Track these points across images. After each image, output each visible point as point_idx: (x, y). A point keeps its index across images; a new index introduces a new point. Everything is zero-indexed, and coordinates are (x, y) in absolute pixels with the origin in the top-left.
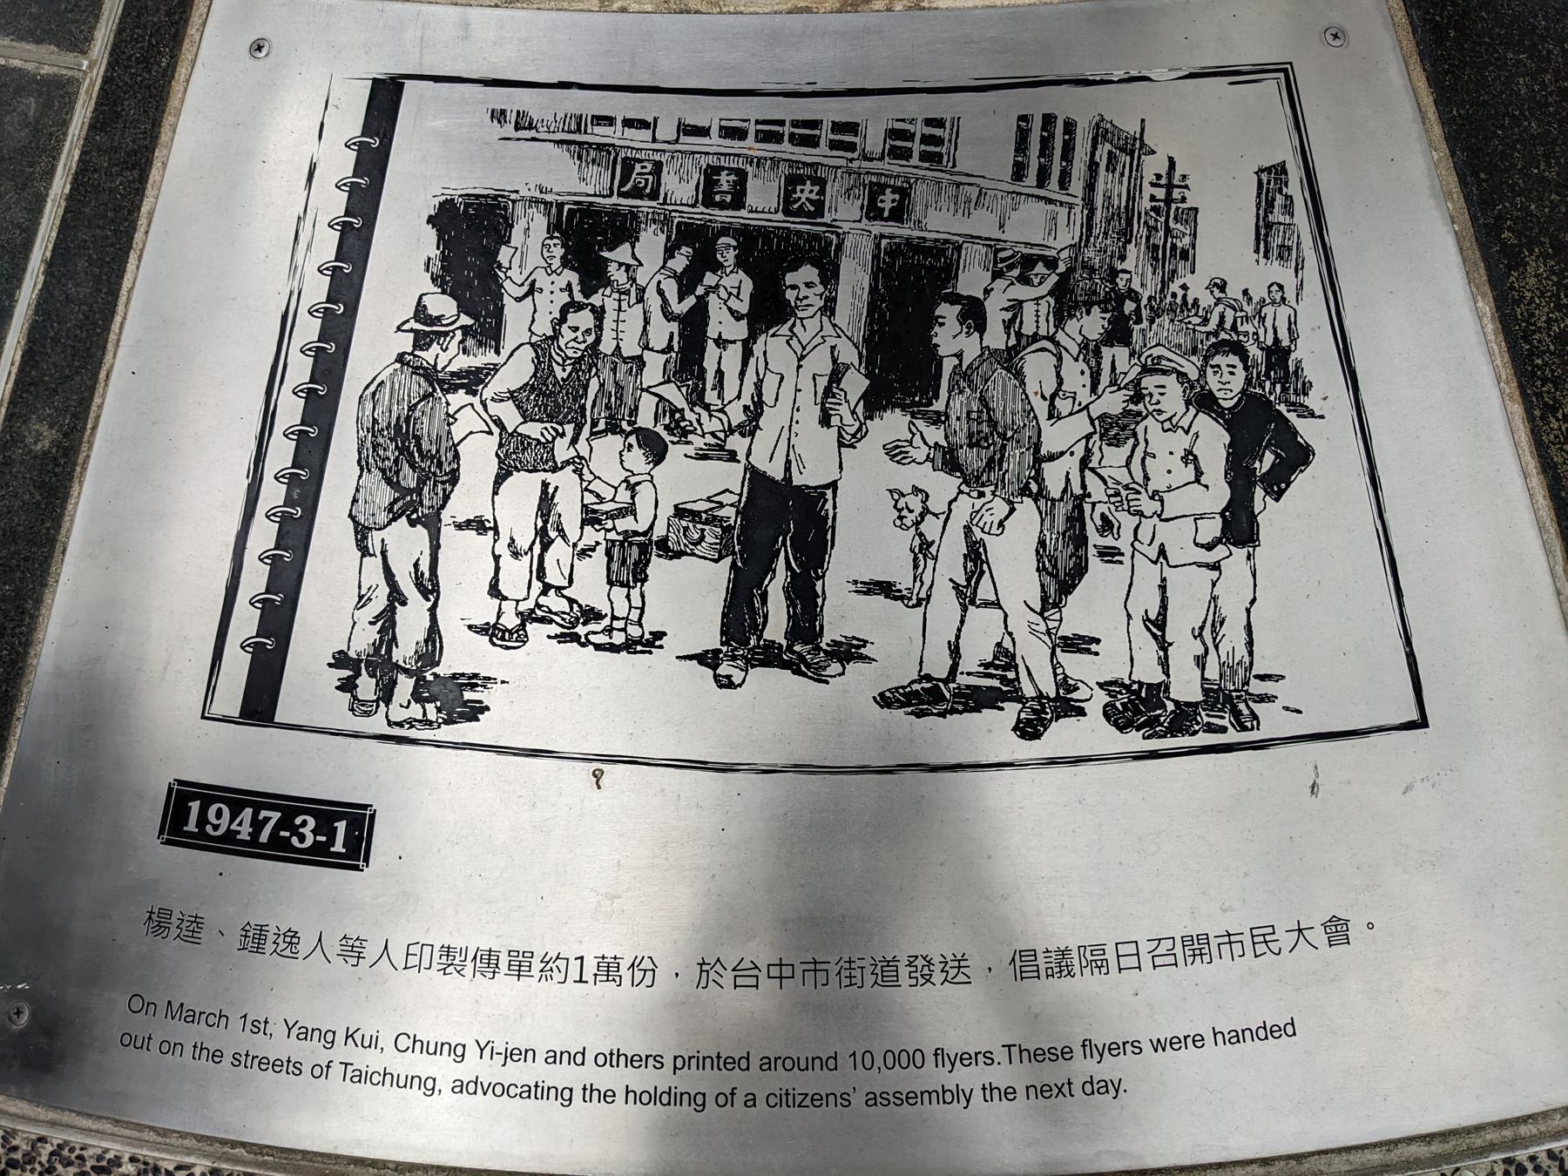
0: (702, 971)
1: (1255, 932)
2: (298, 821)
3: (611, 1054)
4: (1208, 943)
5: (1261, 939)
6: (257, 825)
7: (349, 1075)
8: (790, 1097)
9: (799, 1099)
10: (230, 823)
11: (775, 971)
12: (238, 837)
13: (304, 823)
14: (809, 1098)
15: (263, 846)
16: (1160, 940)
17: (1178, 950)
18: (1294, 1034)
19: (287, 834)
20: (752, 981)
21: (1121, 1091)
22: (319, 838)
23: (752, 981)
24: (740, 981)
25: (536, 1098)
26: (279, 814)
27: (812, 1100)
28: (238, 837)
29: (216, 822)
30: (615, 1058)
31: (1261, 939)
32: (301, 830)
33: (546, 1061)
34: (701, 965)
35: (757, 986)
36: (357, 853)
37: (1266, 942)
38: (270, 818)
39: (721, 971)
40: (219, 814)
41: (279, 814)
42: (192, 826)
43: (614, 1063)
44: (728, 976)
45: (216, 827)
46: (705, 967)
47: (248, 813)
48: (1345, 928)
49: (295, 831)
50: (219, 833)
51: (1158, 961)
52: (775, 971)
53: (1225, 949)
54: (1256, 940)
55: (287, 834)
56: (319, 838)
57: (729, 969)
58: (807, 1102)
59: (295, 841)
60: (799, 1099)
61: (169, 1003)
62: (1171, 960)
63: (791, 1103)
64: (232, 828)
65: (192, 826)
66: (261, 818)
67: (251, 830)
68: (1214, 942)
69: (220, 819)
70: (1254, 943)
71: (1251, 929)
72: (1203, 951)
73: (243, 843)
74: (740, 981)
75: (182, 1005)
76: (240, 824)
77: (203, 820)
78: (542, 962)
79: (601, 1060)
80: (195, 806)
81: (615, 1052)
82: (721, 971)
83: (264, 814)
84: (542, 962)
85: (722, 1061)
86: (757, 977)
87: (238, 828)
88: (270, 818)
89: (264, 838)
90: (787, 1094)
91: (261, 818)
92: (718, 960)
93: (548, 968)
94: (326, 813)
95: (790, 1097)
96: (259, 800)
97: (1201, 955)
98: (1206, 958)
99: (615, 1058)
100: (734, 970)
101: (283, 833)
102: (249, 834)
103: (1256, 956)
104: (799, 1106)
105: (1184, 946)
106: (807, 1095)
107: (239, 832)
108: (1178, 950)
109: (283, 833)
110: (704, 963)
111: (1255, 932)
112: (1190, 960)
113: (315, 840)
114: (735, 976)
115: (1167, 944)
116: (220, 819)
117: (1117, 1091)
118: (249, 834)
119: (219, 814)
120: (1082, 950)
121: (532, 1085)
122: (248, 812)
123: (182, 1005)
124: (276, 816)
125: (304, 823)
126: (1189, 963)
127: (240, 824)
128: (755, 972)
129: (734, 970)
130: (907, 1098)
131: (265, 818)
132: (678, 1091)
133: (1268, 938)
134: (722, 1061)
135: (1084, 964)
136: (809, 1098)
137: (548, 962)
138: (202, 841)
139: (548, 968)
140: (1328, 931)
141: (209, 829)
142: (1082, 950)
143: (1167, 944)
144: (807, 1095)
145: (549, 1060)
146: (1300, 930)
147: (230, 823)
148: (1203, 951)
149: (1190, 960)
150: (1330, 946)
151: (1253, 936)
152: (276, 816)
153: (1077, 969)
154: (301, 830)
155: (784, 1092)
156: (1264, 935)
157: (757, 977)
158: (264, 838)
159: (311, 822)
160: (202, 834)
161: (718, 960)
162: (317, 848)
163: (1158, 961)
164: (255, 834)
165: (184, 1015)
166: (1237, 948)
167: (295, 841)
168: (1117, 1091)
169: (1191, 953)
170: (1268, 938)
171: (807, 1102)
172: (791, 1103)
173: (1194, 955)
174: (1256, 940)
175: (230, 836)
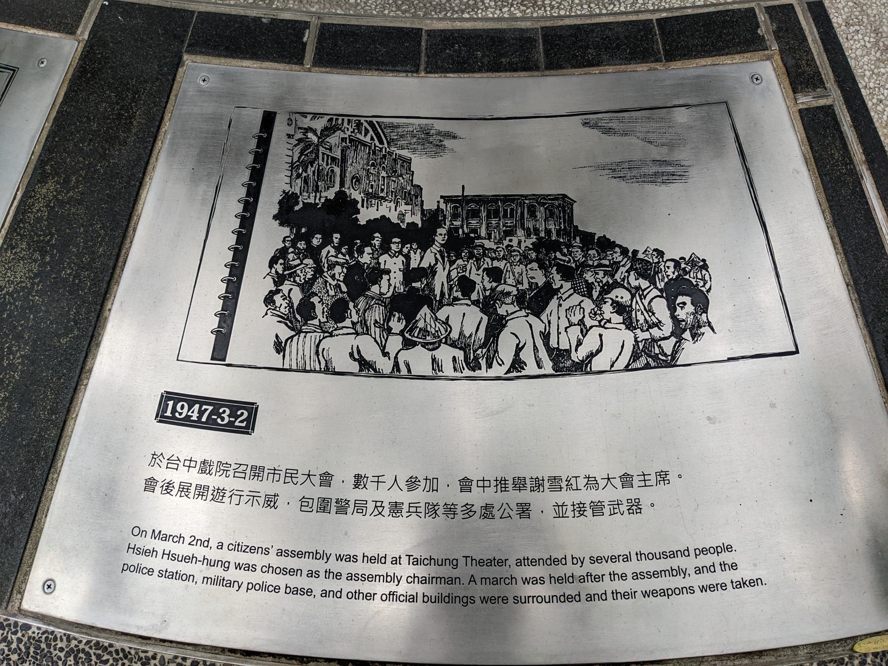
0: (153, 458)
1: (288, 471)
2: (221, 411)
3: (356, 592)
4: (263, 471)
5: (290, 475)
6: (201, 413)
7: (411, 561)
8: (240, 547)
9: (244, 548)
10: (188, 412)
11: (187, 463)
12: (192, 418)
13: (224, 412)
14: (249, 548)
15: (203, 423)
16: (241, 465)
17: (248, 472)
18: (366, 501)
19: (216, 417)
20: (175, 466)
21: (687, 575)
22: (231, 419)
23: (175, 466)
24: (169, 465)
25: (238, 551)
26: (212, 407)
27: (251, 549)
28: (192, 418)
29: (181, 411)
30: (357, 594)
31: (290, 475)
32: (222, 415)
33: (277, 554)
34: (153, 455)
35: (177, 469)
36: (248, 428)
37: (291, 477)
38: (208, 409)
39: (162, 459)
40: (182, 407)
41: (212, 407)
42: (168, 414)
43: (357, 597)
44: (165, 462)
45: (180, 414)
46: (155, 456)
47: (197, 407)
48: (631, 479)
49: (219, 415)
50: (182, 416)
51: (237, 475)
52: (187, 463)
53: (271, 476)
54: (287, 475)
55: (216, 417)
56: (231, 419)
57: (166, 458)
58: (248, 550)
59: (219, 421)
60: (244, 548)
61: (154, 531)
62: (243, 475)
63: (240, 549)
64: (189, 414)
65: (168, 414)
66: (203, 409)
67: (198, 415)
68: (266, 471)
69: (183, 410)
70: (285, 477)
71: (287, 469)
72: (260, 475)
73: (194, 421)
74: (169, 465)
75: (160, 532)
76: (193, 412)
77: (174, 410)
78: (566, 481)
79: (350, 595)
80: (171, 403)
81: (357, 591)
82: (162, 459)
83: (204, 407)
84: (566, 481)
85: (496, 561)
86: (178, 464)
87: (192, 414)
88: (208, 409)
89: (204, 419)
90: (239, 545)
91: (203, 409)
92: (162, 454)
93: (569, 484)
94: (235, 406)
95: (240, 547)
96: (203, 401)
97: (258, 476)
98: (260, 478)
99: (357, 594)
100: (168, 460)
101: (213, 417)
102: (197, 417)
103: (284, 483)
104: (244, 551)
105: (251, 470)
106: (248, 546)
107: (192, 416)
108: (248, 472)
109: (213, 417)
110: (155, 455)
111: (288, 471)
112: (252, 477)
113: (229, 420)
114: (168, 463)
115: (243, 468)
116: (183, 410)
117: (685, 574)
118: (197, 417)
119: (182, 407)
120: (219, 463)
121: (353, 592)
122: (197, 407)
123: (160, 532)
124: (211, 408)
125: (224, 412)
126: (251, 479)
127: (193, 412)
128: (178, 462)
129: (168, 460)
130: (289, 571)
131: (205, 409)
132: (243, 544)
133: (293, 475)
134: (496, 561)
135: (218, 470)
136: (249, 548)
137: (569, 481)
138: (173, 420)
139: (569, 484)
140: (322, 478)
141: (177, 415)
142: (219, 463)
143: (243, 468)
144: (248, 546)
145: (279, 554)
146: (309, 475)
147: (188, 412)
148: (260, 475)
149: (252, 477)
150: (623, 488)
151: (286, 473)
152: (211, 408)
153: (213, 471)
154: (222, 415)
155: (237, 543)
156: (292, 474)
157: (178, 464)
158: (204, 419)
159: (228, 411)
160: (174, 417)
161: (162, 454)
162: (231, 424)
163: (237, 475)
164: (200, 417)
165: (161, 536)
166: (277, 477)
167: (219, 421)
168: (685, 574)
169: (254, 474)
170: (293, 475)
171: (248, 550)
172: (240, 549)
173: (255, 476)
174: (287, 475)
175: (188, 418)
